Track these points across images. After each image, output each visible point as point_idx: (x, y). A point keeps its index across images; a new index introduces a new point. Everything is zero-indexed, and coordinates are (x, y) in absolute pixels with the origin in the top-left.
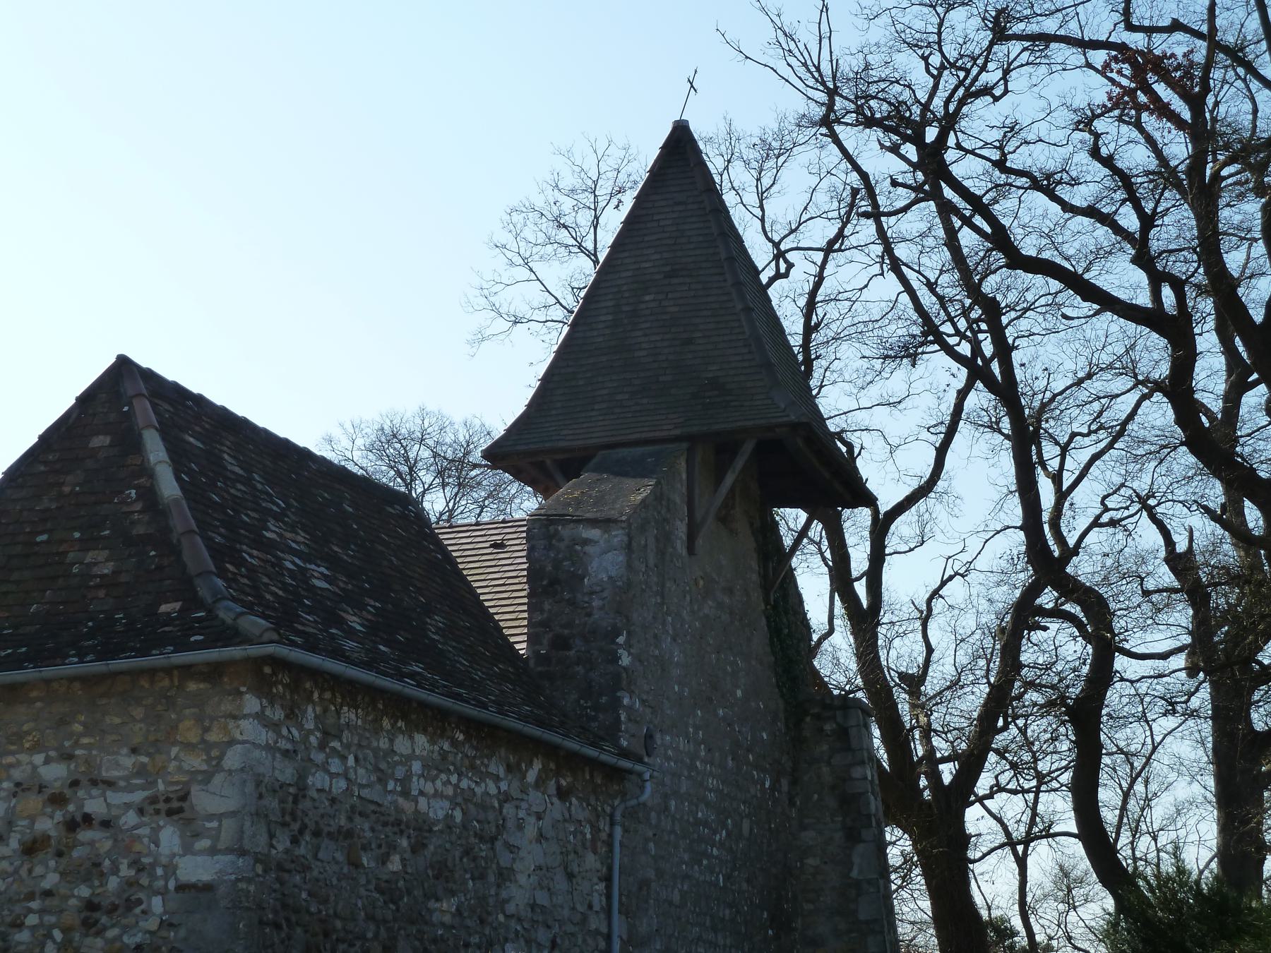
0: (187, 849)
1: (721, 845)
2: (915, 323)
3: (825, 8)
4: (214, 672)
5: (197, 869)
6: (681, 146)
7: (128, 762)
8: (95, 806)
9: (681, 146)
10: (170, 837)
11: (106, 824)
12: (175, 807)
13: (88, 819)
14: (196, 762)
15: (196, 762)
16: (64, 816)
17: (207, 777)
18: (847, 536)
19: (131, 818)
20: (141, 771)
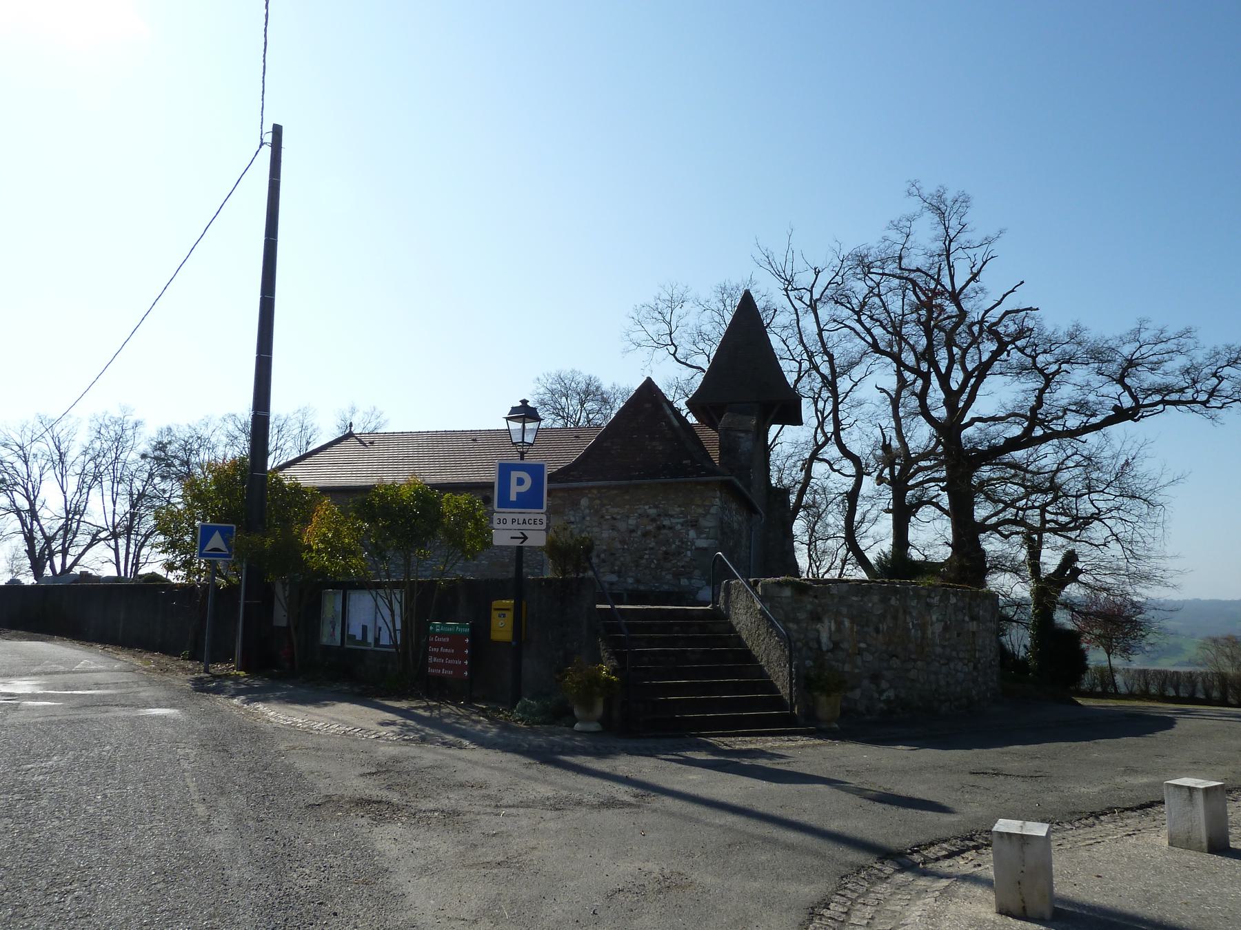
4: (706, 484)
7: (678, 509)
8: (666, 523)
9: (747, 298)
10: (692, 534)
11: (670, 528)
12: (694, 524)
14: (700, 511)
15: (700, 511)
17: (704, 516)
19: (679, 527)
20: (682, 512)
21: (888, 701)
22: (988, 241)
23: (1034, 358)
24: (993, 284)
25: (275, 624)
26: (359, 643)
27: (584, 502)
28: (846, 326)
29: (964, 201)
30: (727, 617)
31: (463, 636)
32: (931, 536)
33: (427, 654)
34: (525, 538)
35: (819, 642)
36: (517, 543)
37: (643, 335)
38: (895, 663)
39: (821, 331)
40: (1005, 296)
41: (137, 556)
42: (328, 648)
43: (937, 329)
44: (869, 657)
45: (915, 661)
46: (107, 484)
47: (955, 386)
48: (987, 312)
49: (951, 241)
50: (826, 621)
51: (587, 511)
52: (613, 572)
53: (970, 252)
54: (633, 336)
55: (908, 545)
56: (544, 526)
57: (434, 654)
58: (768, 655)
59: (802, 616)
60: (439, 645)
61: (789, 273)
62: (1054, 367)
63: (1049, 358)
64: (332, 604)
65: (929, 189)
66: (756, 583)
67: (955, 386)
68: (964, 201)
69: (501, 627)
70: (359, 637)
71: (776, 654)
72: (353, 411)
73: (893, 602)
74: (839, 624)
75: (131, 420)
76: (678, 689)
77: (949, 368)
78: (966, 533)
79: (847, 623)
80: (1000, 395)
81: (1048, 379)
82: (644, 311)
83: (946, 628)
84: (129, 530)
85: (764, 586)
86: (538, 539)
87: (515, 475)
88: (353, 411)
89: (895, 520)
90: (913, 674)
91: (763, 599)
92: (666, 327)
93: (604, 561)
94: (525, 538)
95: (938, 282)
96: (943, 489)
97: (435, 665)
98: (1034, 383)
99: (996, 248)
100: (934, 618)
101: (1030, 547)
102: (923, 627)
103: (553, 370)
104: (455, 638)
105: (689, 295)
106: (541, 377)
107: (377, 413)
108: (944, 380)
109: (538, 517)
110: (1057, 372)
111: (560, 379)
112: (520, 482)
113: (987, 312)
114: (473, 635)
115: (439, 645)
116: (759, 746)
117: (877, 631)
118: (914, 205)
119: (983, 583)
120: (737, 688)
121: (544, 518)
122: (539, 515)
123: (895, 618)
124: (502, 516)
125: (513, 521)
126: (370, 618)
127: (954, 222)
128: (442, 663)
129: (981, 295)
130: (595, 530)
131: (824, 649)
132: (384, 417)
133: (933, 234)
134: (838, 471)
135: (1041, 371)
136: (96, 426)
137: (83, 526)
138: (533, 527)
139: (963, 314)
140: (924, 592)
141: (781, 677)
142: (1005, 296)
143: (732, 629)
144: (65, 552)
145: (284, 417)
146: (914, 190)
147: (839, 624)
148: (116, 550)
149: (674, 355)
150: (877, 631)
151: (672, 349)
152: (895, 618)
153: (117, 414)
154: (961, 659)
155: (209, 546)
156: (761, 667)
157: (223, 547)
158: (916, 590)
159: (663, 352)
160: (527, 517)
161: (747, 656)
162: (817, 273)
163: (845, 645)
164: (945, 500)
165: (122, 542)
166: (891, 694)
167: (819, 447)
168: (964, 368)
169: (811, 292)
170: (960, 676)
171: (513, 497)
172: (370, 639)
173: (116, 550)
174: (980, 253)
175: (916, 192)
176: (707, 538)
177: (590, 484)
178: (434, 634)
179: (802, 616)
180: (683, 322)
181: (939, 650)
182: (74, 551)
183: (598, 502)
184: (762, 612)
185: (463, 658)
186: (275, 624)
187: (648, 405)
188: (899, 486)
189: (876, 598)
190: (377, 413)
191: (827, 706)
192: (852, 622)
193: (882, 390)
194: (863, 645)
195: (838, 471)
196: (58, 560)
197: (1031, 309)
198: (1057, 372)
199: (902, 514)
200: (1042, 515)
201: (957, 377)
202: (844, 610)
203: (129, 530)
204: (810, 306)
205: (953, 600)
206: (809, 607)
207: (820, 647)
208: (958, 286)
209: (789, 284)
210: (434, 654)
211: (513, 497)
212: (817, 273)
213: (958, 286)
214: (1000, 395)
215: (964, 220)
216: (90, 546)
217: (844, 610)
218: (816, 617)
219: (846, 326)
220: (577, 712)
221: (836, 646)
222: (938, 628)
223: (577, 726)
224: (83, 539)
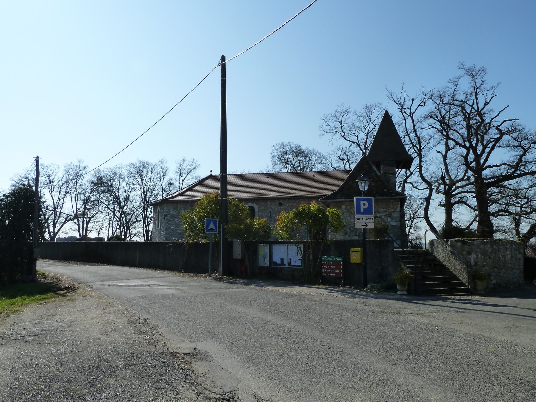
0: (392, 221)
1: (209, 209)
2: (497, 134)
3: (223, 58)
4: (394, 199)
5: (393, 223)
6: (387, 113)
7: (383, 210)
8: (378, 215)
9: (387, 113)
10: (389, 219)
11: (380, 217)
12: (390, 216)
13: (377, 217)
14: (392, 210)
15: (392, 210)
16: (319, 211)
17: (394, 212)
18: (359, 160)
19: (383, 217)
20: (385, 211)
21: (494, 284)
22: (493, 88)
23: (520, 142)
24: (495, 106)
25: (234, 257)
26: (279, 265)
27: (343, 207)
28: (433, 127)
29: (483, 70)
30: (432, 253)
31: (340, 261)
32: (465, 216)
33: (322, 268)
34: (367, 225)
35: (470, 262)
36: (364, 227)
37: (328, 127)
38: (496, 270)
39: (414, 126)
40: (500, 112)
41: (87, 227)
42: (262, 268)
43: (475, 130)
44: (487, 268)
45: (502, 269)
46: (73, 195)
47: (479, 152)
48: (492, 119)
49: (477, 88)
50: (473, 254)
51: (345, 211)
52: (356, 235)
53: (484, 93)
54: (324, 128)
55: (452, 221)
56: (373, 221)
57: (325, 268)
58: (455, 267)
59: (464, 253)
60: (327, 265)
61: (402, 102)
62: (528, 146)
63: (526, 142)
64: (263, 250)
65: (468, 65)
66: (448, 241)
67: (479, 152)
68: (483, 70)
69: (356, 256)
70: (279, 262)
71: (459, 267)
72: (184, 161)
73: (495, 247)
74: (477, 256)
75: (83, 166)
76: (427, 280)
77: (477, 145)
78: (484, 217)
79: (480, 255)
80: (500, 157)
81: (525, 151)
82: (329, 117)
83: (512, 257)
84: (83, 215)
85: (451, 242)
86: (371, 226)
87: (362, 202)
88: (184, 161)
89: (446, 210)
90: (501, 274)
91: (450, 246)
92: (339, 124)
93: (352, 231)
94: (367, 225)
95: (473, 108)
96: (474, 197)
97: (325, 272)
98: (520, 152)
99: (497, 91)
100: (508, 253)
101: (516, 222)
102: (504, 256)
103: (280, 142)
104: (335, 263)
105: (350, 110)
106: (275, 145)
107: (195, 161)
108: (475, 149)
109: (371, 217)
110: (529, 148)
111: (284, 146)
112: (364, 205)
113: (492, 119)
114: (344, 261)
115: (327, 265)
116: (470, 298)
117: (490, 258)
118: (462, 72)
119: (493, 237)
120: (445, 279)
121: (373, 218)
122: (372, 216)
123: (495, 253)
124: (358, 217)
125: (362, 219)
126: (290, 255)
127: (479, 80)
128: (327, 270)
129: (491, 113)
130: (348, 218)
131: (472, 264)
132: (198, 163)
133: (469, 85)
134: (416, 187)
135: (522, 147)
136: (66, 168)
137: (62, 214)
138: (369, 221)
139: (483, 120)
140: (505, 243)
141: (463, 276)
142: (500, 112)
143: (435, 257)
144: (55, 226)
145: (154, 164)
146: (461, 66)
147: (477, 256)
148: (78, 225)
149: (343, 136)
150: (490, 258)
151: (343, 134)
152: (495, 253)
153: (77, 163)
154: (516, 269)
155: (210, 228)
156: (451, 272)
157: (214, 228)
158: (346, 233)
159: (339, 135)
160: (367, 218)
161: (444, 268)
162: (413, 100)
163: (479, 264)
164: (474, 202)
165: (81, 220)
166: (494, 281)
167: (408, 177)
168: (482, 144)
169: (410, 109)
170: (516, 275)
171: (362, 210)
172: (285, 263)
173: (78, 225)
174: (489, 94)
175: (462, 67)
176: (396, 221)
177: (347, 200)
178: (325, 261)
179: (464, 253)
180: (347, 122)
181: (510, 265)
182: (58, 226)
183: (349, 207)
184: (451, 251)
185: (340, 269)
186: (234, 257)
187: (366, 166)
188: (448, 194)
189: (489, 246)
190: (195, 161)
191: (480, 285)
192: (481, 255)
193: (439, 152)
194: (485, 263)
195: (416, 187)
196: (51, 229)
197: (516, 119)
198: (529, 148)
199: (449, 208)
200: (521, 209)
201: (480, 148)
202: (478, 250)
203: (83, 215)
204: (410, 116)
205: (514, 246)
206: (467, 249)
207: (471, 264)
208: (480, 109)
209: (402, 108)
210: (325, 268)
211: (362, 210)
212: (413, 100)
213: (480, 109)
214: (500, 157)
215: (483, 79)
216: (64, 223)
217: (478, 250)
218: (469, 253)
219: (433, 127)
220: (398, 287)
221: (476, 264)
222: (509, 257)
223: (398, 292)
224: (62, 220)
